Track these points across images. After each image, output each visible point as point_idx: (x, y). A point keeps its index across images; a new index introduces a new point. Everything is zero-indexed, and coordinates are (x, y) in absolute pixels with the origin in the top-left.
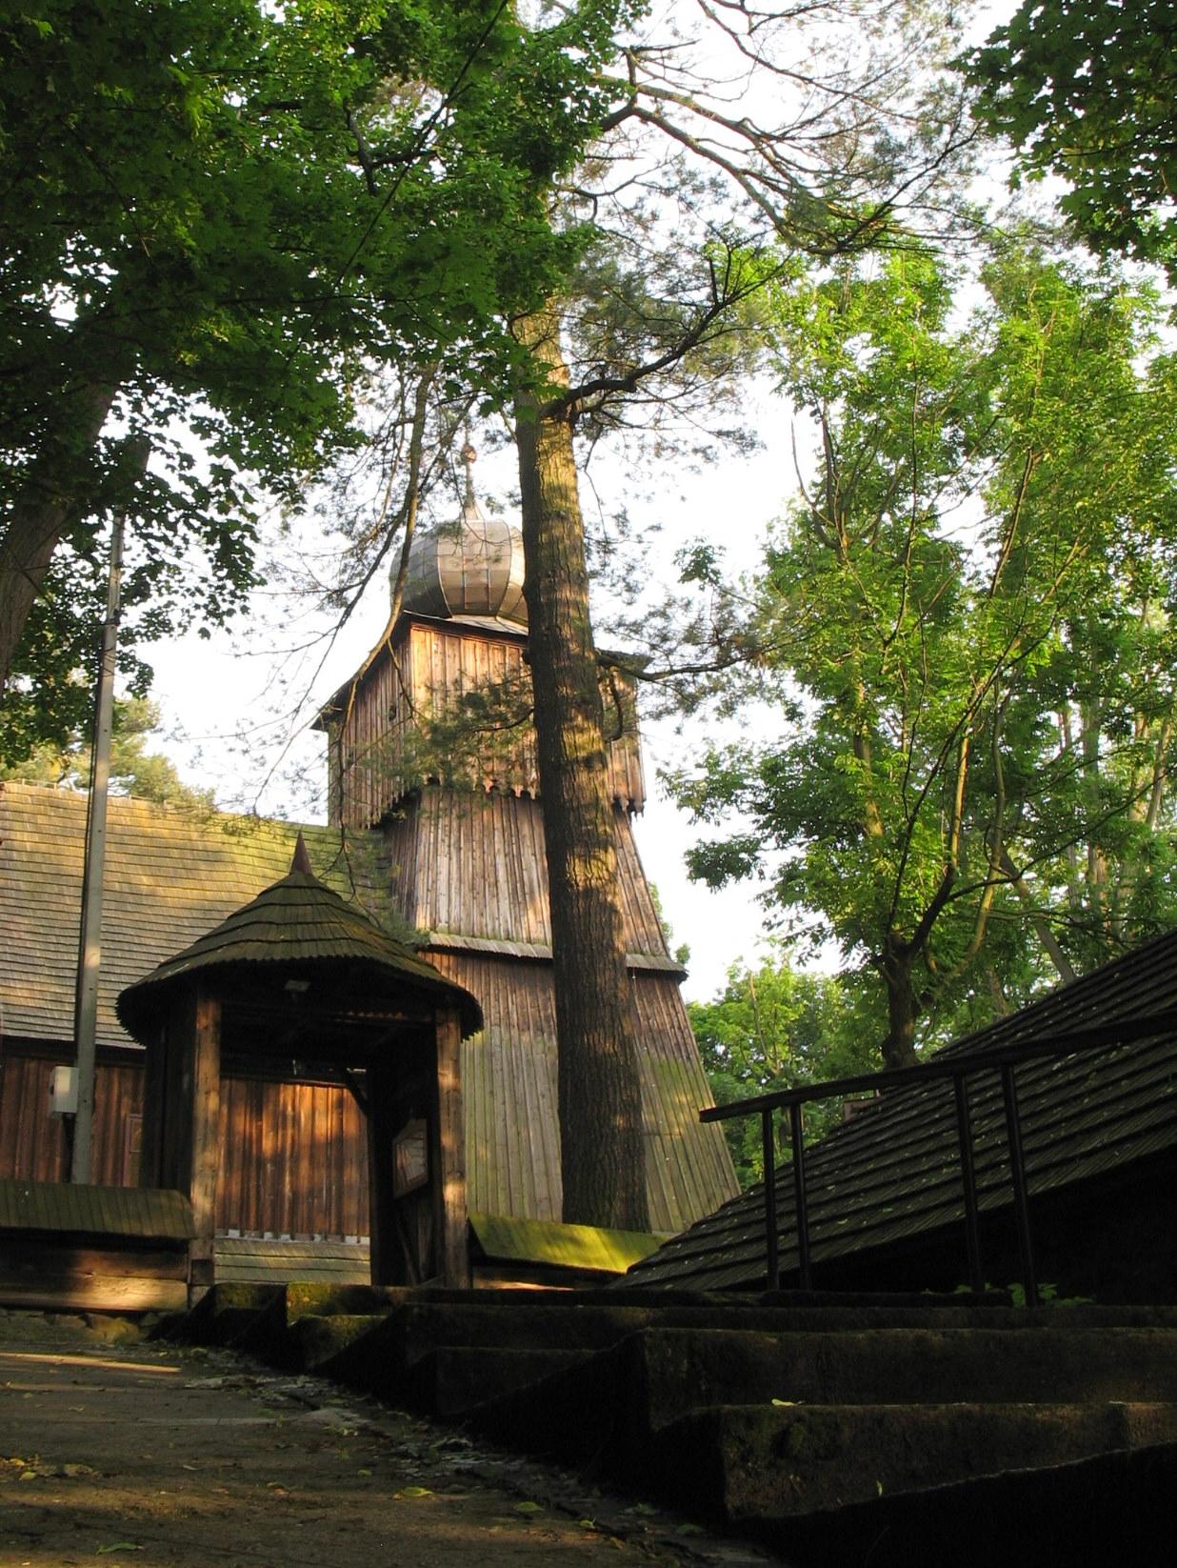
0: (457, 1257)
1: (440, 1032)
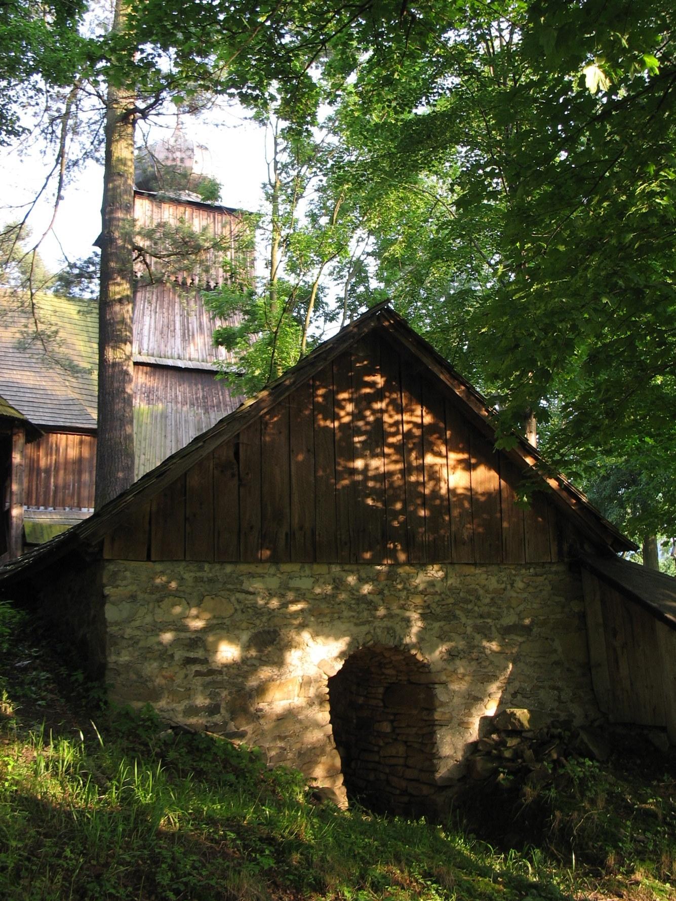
0: (16, 542)
1: (15, 438)
